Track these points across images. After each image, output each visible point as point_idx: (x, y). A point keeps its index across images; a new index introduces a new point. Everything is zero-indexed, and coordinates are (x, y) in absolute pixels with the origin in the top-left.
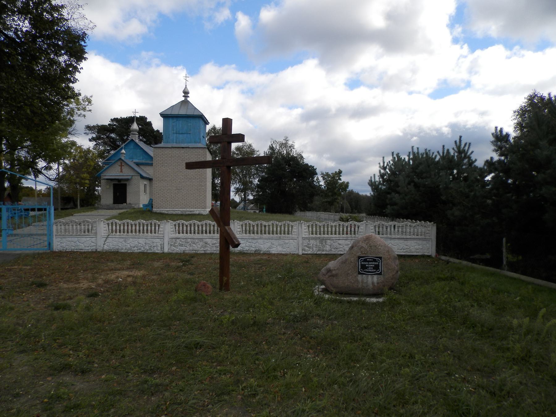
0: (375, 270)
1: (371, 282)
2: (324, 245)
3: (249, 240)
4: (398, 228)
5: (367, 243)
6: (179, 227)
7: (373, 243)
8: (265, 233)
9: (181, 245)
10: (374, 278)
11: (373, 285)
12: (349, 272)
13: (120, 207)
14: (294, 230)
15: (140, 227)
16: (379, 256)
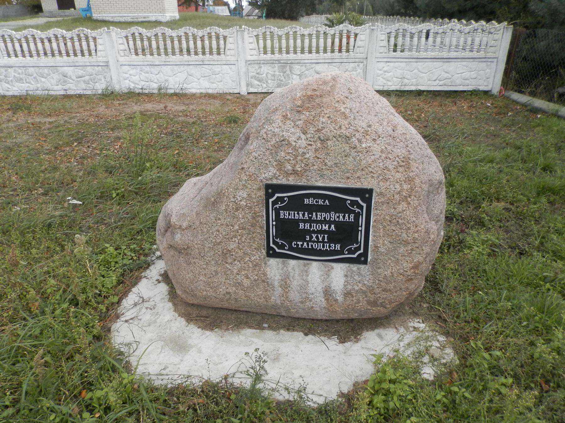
0: (338, 247)
1: (320, 289)
2: (288, 75)
3: (144, 67)
4: (435, 37)
5: (307, 122)
6: (265, 40)
7: (335, 122)
8: (174, 53)
9: (20, 80)
10: (333, 274)
11: (327, 300)
12: (232, 246)
13: (66, 14)
14: (360, 43)
15: (188, 42)
16: (358, 185)
